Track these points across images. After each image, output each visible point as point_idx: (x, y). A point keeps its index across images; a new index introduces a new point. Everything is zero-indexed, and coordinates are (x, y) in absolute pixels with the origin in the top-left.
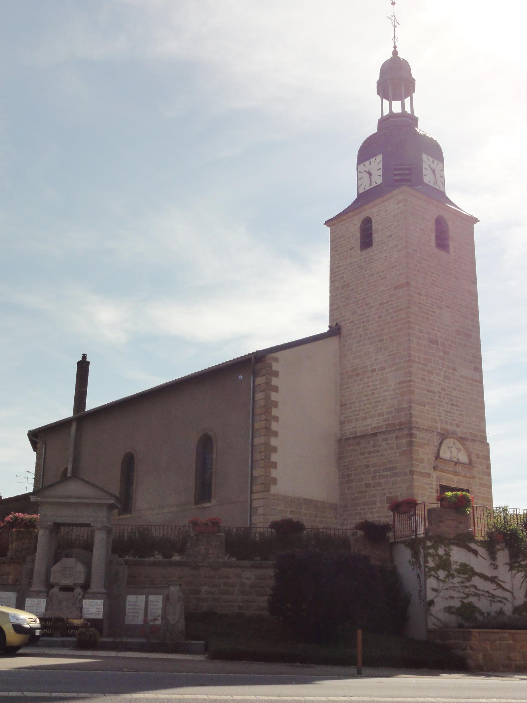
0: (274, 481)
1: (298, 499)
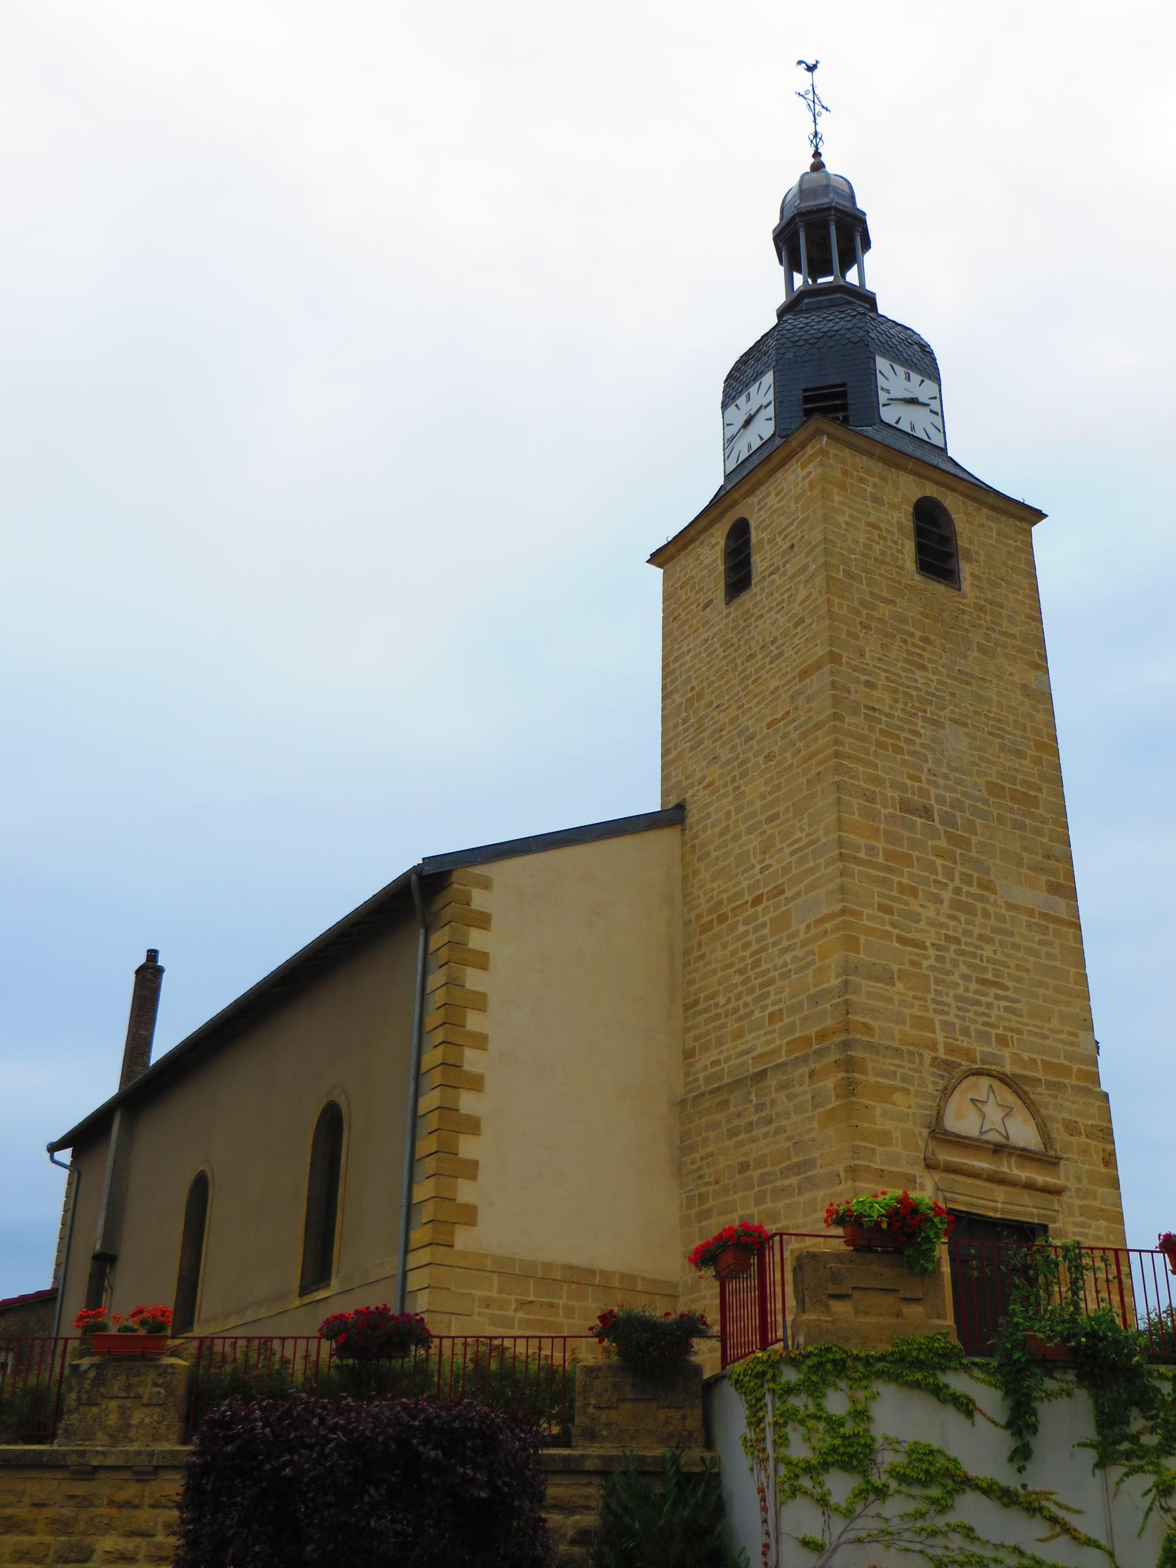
0: (469, 1215)
1: (548, 1266)
